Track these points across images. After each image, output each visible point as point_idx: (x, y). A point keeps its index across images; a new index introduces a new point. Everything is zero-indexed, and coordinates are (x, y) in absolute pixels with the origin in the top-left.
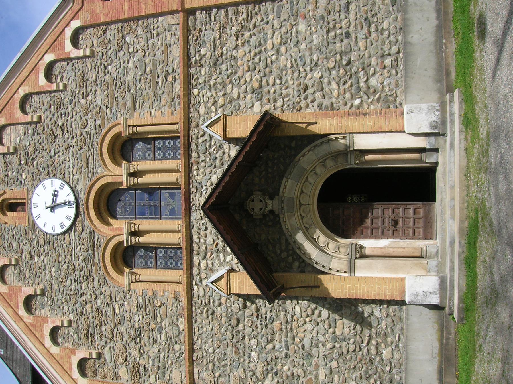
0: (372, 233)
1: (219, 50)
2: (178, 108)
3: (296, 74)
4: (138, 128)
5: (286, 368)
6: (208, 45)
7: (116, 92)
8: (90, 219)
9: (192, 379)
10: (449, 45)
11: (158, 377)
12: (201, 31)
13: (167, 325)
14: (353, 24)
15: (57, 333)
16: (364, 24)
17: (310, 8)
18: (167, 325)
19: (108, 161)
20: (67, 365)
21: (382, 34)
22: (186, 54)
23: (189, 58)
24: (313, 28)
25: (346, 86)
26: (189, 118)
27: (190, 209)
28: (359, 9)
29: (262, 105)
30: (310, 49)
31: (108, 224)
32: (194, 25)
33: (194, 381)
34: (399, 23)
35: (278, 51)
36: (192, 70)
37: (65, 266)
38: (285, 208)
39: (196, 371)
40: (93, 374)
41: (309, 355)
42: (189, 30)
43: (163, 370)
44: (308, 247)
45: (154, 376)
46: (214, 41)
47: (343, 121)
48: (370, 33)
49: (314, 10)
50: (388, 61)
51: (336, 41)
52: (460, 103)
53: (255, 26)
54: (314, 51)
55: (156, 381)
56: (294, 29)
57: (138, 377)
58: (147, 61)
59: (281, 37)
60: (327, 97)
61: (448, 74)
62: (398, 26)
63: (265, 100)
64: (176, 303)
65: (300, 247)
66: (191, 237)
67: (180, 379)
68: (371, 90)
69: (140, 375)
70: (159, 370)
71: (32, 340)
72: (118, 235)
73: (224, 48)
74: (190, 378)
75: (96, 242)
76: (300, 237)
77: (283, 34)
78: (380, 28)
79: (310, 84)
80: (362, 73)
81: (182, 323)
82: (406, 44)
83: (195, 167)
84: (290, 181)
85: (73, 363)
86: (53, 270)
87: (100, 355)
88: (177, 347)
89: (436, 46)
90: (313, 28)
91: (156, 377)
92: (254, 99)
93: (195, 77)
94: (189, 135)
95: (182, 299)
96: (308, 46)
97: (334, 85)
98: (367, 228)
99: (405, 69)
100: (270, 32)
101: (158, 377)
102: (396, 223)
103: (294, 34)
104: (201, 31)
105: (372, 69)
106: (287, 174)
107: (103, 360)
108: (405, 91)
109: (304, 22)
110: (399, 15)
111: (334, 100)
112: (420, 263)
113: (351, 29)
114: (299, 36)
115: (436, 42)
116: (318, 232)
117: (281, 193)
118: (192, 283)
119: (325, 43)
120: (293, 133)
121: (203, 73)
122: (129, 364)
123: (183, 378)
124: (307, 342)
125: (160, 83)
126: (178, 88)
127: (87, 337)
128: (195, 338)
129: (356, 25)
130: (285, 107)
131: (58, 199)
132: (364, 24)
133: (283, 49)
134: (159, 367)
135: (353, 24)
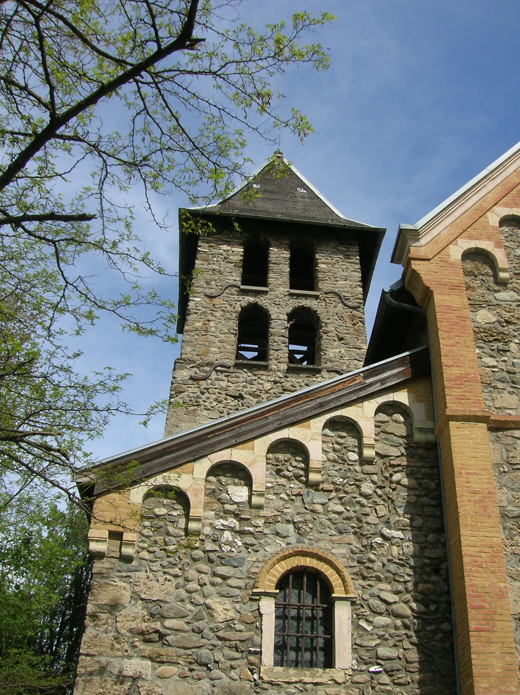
9: (512, 425)
11: (496, 370)
13: (514, 385)
15: (515, 226)
18: (514, 385)
20: (475, 233)
33: (508, 429)
40: (468, 270)
43: (508, 379)
45: (495, 363)
55: (489, 367)
57: (485, 339)
67: (505, 405)
69: (490, 342)
70: (509, 372)
71: (497, 191)
74: (514, 422)
85: (482, 242)
87: (503, 284)
91: (494, 367)
101: (496, 370)
107: (496, 288)
112: (158, 488)
122: (504, 327)
123: (508, 411)
134: (515, 373)
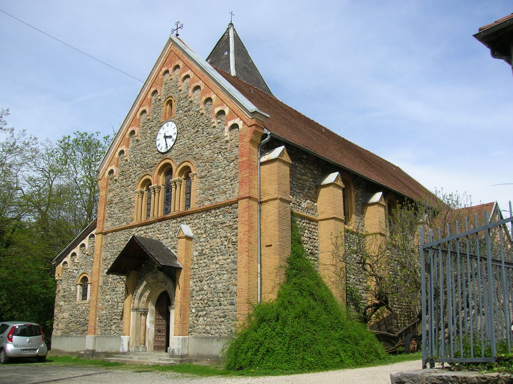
0: (157, 319)
1: (220, 226)
2: (199, 205)
3: (207, 275)
5: (110, 279)
6: (223, 219)
8: (160, 163)
10: (207, 362)
12: (231, 213)
14: (224, 308)
19: (181, 167)
23: (218, 208)
26: (193, 214)
27: (161, 221)
30: (215, 283)
31: (160, 172)
36: (213, 211)
39: (110, 234)
41: (114, 290)
44: (142, 287)
46: (225, 223)
50: (208, 328)
52: (164, 364)
53: (229, 248)
56: (225, 272)
63: (199, 258)
65: (141, 284)
66: (151, 224)
76: (145, 283)
80: (204, 313)
83: (175, 221)
92: (199, 251)
93: (210, 214)
94: (187, 215)
97: (201, 297)
99: (206, 337)
102: (159, 331)
104: (231, 213)
108: (196, 337)
110: (226, 335)
115: (212, 355)
116: (149, 292)
119: (218, 291)
120: (177, 276)
124: (117, 289)
125: (210, 192)
126: (207, 204)
133: (218, 266)
135: (224, 308)
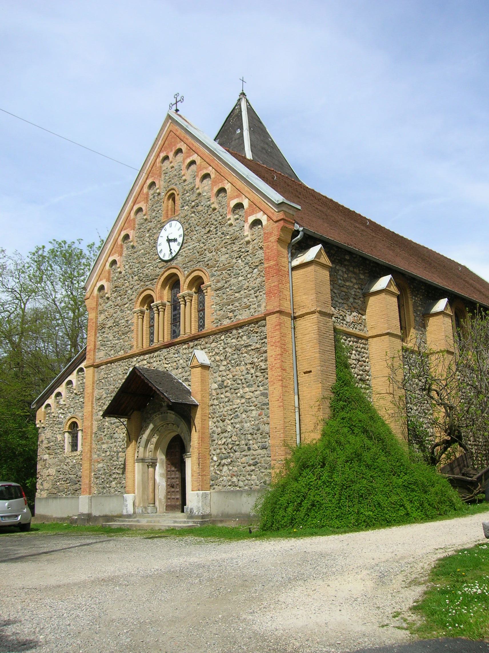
1: (244, 350)
3: (230, 412)
4: (184, 305)
5: (107, 424)
6: (248, 341)
7: (226, 271)
14: (254, 453)
16: (254, 461)
17: (265, 418)
19: (190, 278)
21: (249, 475)
22: (242, 324)
23: (241, 327)
24: (253, 423)
25: (223, 450)
26: (209, 336)
27: (168, 347)
28: (262, 457)
29: (216, 389)
31: (164, 286)
32: (260, 326)
34: (254, 487)
35: (242, 397)
36: (234, 332)
37: (144, 260)
38: (163, 415)
39: (103, 367)
42: (257, 322)
46: (250, 345)
47: (196, 450)
48: (250, 466)
49: (263, 422)
50: (235, 479)
51: (247, 440)
52: (180, 527)
53: (257, 377)
54: (240, 424)
56: (253, 408)
58: (242, 292)
59: (249, 399)
60: (218, 436)
61: (221, 521)
62: (252, 486)
63: (219, 391)
64: (129, 347)
65: (147, 427)
68: (221, 468)
72: (202, 272)
73: (246, 354)
75: (154, 281)
76: (151, 426)
77: (252, 399)
78: (252, 473)
79: (225, 423)
81: (121, 354)
82: (241, 492)
84: (174, 416)
86: (143, 251)
88: (112, 352)
89: (239, 514)
90: (253, 423)
94: (201, 338)
95: (131, 351)
96: (243, 420)
97: (224, 440)
98: (171, 468)
99: (232, 492)
100: (253, 389)
102: (172, 487)
103: (251, 408)
105: (231, 468)
106: (176, 414)
108: (220, 492)
109: (257, 415)
111: (216, 442)
113: (252, 451)
114: (250, 412)
115: (242, 514)
116: (157, 437)
117: (169, 411)
118: (137, 356)
119: (245, 433)
121: (233, 340)
125: (229, 307)
127: (115, 287)
128: (116, 364)
129: (254, 455)
130: (214, 407)
131: (173, 243)
132: (254, 461)
133: (243, 400)
135: (254, 453)
